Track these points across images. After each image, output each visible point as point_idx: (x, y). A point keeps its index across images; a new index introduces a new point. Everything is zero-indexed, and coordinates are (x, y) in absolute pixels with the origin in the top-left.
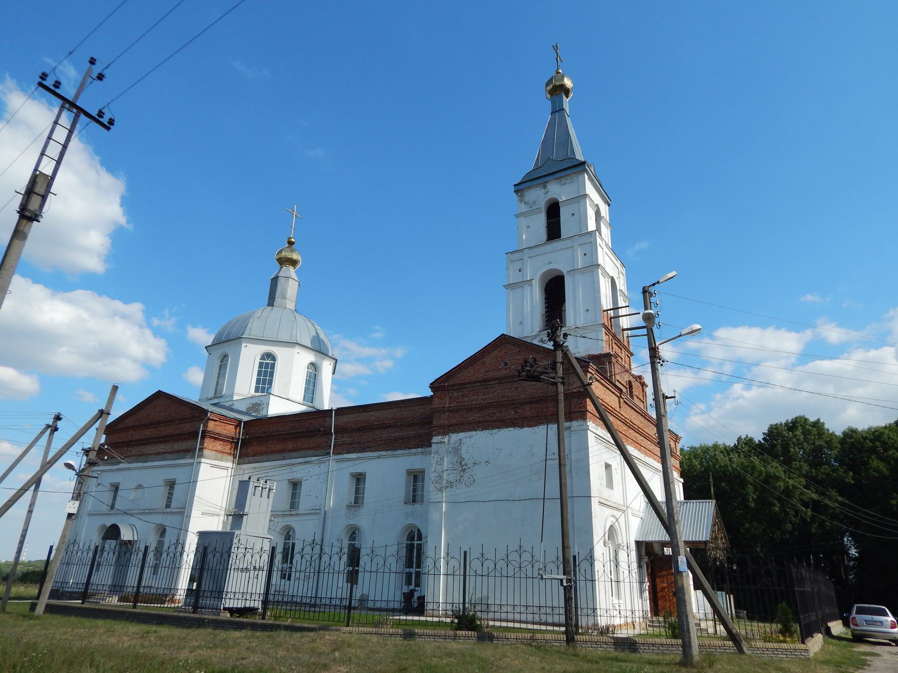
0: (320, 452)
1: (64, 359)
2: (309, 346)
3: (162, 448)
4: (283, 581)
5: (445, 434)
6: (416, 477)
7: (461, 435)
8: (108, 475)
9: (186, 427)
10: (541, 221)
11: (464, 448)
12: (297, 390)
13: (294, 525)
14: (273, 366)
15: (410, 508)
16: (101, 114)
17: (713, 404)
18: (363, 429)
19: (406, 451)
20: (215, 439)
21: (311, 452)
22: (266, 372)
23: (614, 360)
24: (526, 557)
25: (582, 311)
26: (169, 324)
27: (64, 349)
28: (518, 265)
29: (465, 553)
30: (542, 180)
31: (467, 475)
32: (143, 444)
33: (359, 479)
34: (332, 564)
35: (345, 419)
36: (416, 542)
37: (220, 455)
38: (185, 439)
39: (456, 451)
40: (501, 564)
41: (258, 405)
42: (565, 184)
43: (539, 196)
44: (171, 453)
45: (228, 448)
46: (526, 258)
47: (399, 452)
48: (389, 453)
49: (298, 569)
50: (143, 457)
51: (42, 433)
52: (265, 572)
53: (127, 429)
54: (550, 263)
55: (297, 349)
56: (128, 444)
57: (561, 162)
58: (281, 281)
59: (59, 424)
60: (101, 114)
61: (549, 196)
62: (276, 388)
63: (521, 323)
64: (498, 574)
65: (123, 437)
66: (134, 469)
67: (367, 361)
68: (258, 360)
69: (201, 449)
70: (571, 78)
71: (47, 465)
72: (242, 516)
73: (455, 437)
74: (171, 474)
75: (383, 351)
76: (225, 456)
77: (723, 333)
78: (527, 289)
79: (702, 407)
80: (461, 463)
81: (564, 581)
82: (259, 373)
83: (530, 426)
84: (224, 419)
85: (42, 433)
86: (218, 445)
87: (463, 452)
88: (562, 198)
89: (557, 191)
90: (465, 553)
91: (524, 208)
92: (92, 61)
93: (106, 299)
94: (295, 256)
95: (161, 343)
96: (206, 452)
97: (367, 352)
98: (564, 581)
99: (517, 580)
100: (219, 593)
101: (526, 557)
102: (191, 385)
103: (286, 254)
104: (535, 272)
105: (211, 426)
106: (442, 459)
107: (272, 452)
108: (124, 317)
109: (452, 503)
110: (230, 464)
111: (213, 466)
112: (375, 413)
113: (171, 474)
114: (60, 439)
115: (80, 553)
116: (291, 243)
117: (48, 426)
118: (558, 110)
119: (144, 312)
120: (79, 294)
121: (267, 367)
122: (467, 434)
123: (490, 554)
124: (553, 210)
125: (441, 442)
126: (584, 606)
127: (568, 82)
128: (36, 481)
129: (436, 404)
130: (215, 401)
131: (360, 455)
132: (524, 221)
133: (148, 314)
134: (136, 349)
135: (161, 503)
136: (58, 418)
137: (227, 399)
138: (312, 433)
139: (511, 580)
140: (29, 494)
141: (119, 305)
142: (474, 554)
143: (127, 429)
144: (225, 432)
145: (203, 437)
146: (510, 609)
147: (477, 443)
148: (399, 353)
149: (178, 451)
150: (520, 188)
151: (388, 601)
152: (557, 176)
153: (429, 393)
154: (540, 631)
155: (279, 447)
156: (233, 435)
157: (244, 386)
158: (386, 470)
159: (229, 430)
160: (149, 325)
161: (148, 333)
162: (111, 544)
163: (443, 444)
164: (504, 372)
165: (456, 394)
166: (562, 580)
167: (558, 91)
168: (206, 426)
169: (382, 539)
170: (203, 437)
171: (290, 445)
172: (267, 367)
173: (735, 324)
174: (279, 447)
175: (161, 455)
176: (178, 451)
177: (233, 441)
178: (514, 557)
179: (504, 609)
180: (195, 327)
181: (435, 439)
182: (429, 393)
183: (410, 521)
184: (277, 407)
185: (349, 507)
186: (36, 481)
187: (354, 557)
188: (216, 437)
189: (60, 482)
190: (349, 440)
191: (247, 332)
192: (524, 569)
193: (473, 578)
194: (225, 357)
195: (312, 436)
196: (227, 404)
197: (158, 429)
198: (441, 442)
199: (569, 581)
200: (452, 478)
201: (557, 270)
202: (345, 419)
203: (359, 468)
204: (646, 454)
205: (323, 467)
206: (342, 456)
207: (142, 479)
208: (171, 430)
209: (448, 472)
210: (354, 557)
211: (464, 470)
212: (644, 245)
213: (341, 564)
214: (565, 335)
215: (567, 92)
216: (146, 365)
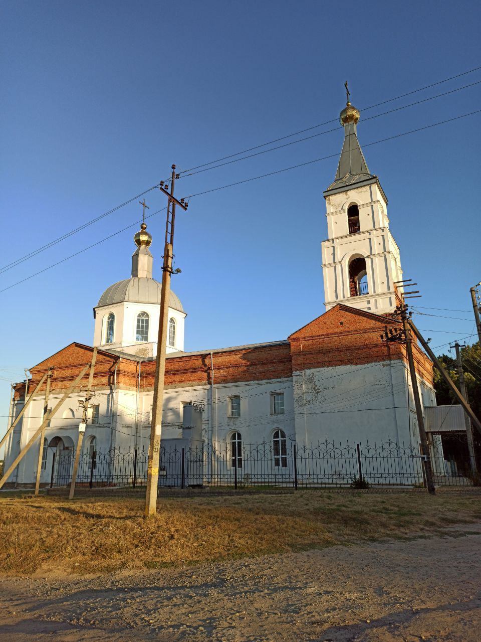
2: (182, 310)
7: (313, 370)
11: (316, 379)
14: (147, 321)
16: (182, 200)
22: (142, 326)
31: (319, 396)
34: (252, 455)
36: (237, 441)
37: (128, 387)
39: (310, 380)
40: (379, 451)
41: (145, 350)
42: (361, 192)
45: (132, 382)
54: (354, 250)
60: (182, 200)
73: (308, 372)
80: (314, 388)
81: (426, 458)
86: (126, 380)
90: (358, 445)
92: (174, 167)
96: (121, 385)
98: (426, 458)
115: (121, 456)
121: (143, 322)
122: (318, 369)
123: (372, 445)
125: (299, 375)
137: (118, 346)
139: (259, 462)
142: (187, 450)
159: (132, 368)
164: (341, 328)
166: (424, 458)
177: (136, 376)
178: (261, 447)
181: (294, 373)
183: (276, 426)
187: (94, 455)
188: (126, 374)
192: (392, 453)
193: (300, 460)
198: (299, 375)
199: (428, 458)
201: (359, 254)
209: (306, 394)
210: (94, 455)
211: (317, 393)
213: (87, 459)
214: (410, 313)
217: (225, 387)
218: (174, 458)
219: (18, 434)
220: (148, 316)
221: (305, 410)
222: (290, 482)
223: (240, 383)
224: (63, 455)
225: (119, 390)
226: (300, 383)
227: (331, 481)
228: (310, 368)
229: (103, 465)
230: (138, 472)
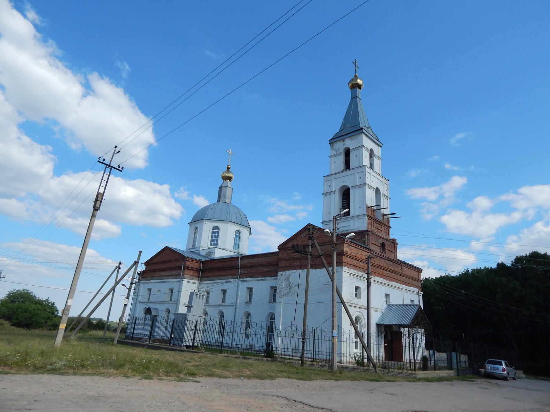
0: (234, 277)
1: (133, 216)
3: (168, 273)
4: (246, 339)
5: (283, 271)
6: (274, 290)
8: (145, 286)
9: (178, 264)
10: (341, 159)
11: (291, 278)
12: (230, 245)
13: (223, 311)
14: (218, 233)
15: (271, 305)
17: (521, 236)
18: (252, 266)
19: (270, 278)
20: (190, 270)
21: (230, 277)
22: (215, 236)
23: (369, 233)
25: (357, 207)
26: (184, 195)
27: (132, 211)
28: (329, 183)
30: (342, 138)
31: (292, 291)
32: (161, 271)
33: (251, 290)
35: (245, 261)
37: (192, 277)
38: (177, 270)
39: (288, 279)
40: (258, 330)
43: (340, 146)
44: (171, 276)
45: (196, 274)
46: (333, 179)
47: (267, 278)
48: (263, 278)
49: (320, 338)
50: (161, 277)
52: (264, 336)
53: (154, 264)
55: (230, 224)
56: (154, 271)
57: (352, 127)
58: (224, 188)
59: (121, 266)
61: (346, 146)
62: (220, 244)
63: (329, 213)
65: (152, 267)
66: (157, 282)
67: (292, 213)
68: (211, 230)
70: (361, 79)
71: (117, 283)
72: (191, 307)
73: (288, 272)
74: (171, 285)
75: (301, 207)
76: (194, 278)
77: (525, 190)
78: (332, 195)
79: (515, 238)
82: (212, 237)
83: (319, 268)
84: (193, 260)
86: (191, 273)
87: (291, 280)
88: (351, 147)
89: (350, 143)
91: (333, 153)
93: (151, 183)
94: (230, 175)
95: (179, 206)
97: (292, 208)
99: (326, 342)
100: (182, 339)
102: (180, 245)
103: (226, 174)
104: (336, 185)
105: (188, 263)
106: (282, 283)
107: (215, 276)
108: (160, 192)
109: (286, 303)
110: (197, 281)
111: (189, 282)
112: (257, 259)
113: (171, 285)
116: (228, 168)
117: (117, 267)
118: (354, 98)
119: (169, 189)
120: (138, 182)
124: (347, 153)
126: (317, 350)
127: (359, 81)
128: (113, 289)
129: (280, 256)
130: (193, 250)
131: (251, 279)
132: (333, 159)
133: (172, 191)
134: (166, 210)
135: (167, 299)
136: (120, 264)
138: (231, 268)
139: (323, 341)
140: (110, 296)
141: (157, 186)
143: (154, 264)
144: (194, 266)
146: (286, 350)
147: (296, 276)
148: (310, 208)
149: (174, 275)
150: (332, 142)
151: (242, 345)
152: (349, 135)
153: (277, 250)
154: (287, 358)
155: (217, 274)
156: (198, 268)
157: (205, 243)
158: (261, 286)
160: (173, 197)
161: (172, 201)
163: (283, 275)
165: (289, 252)
167: (355, 86)
168: (185, 263)
169: (259, 319)
170: (184, 269)
171: (222, 273)
172: (215, 233)
173: (532, 183)
174: (217, 274)
175: (167, 277)
176: (174, 275)
177: (197, 270)
179: (289, 350)
180: (198, 196)
181: (279, 273)
182: (277, 250)
184: (218, 254)
185: (246, 303)
186: (113, 289)
188: (190, 269)
189: (121, 291)
190: (246, 271)
191: (206, 216)
193: (236, 334)
194: (196, 228)
195: (231, 269)
196: (197, 252)
197: (165, 264)
200: (286, 292)
202: (245, 261)
203: (250, 285)
204: (390, 280)
205: (236, 284)
206: (243, 279)
207: (160, 286)
208: (171, 265)
211: (291, 288)
212: (461, 136)
215: (359, 86)
216: (172, 218)
217: (266, 280)
218: (320, 336)
219: (175, 305)
220: (219, 229)
221: (282, 300)
222: (309, 358)
223: (254, 279)
224: (255, 327)
225: (184, 280)
226: (128, 290)
227: (291, 354)
228: (289, 270)
229: (254, 336)
230: (308, 347)
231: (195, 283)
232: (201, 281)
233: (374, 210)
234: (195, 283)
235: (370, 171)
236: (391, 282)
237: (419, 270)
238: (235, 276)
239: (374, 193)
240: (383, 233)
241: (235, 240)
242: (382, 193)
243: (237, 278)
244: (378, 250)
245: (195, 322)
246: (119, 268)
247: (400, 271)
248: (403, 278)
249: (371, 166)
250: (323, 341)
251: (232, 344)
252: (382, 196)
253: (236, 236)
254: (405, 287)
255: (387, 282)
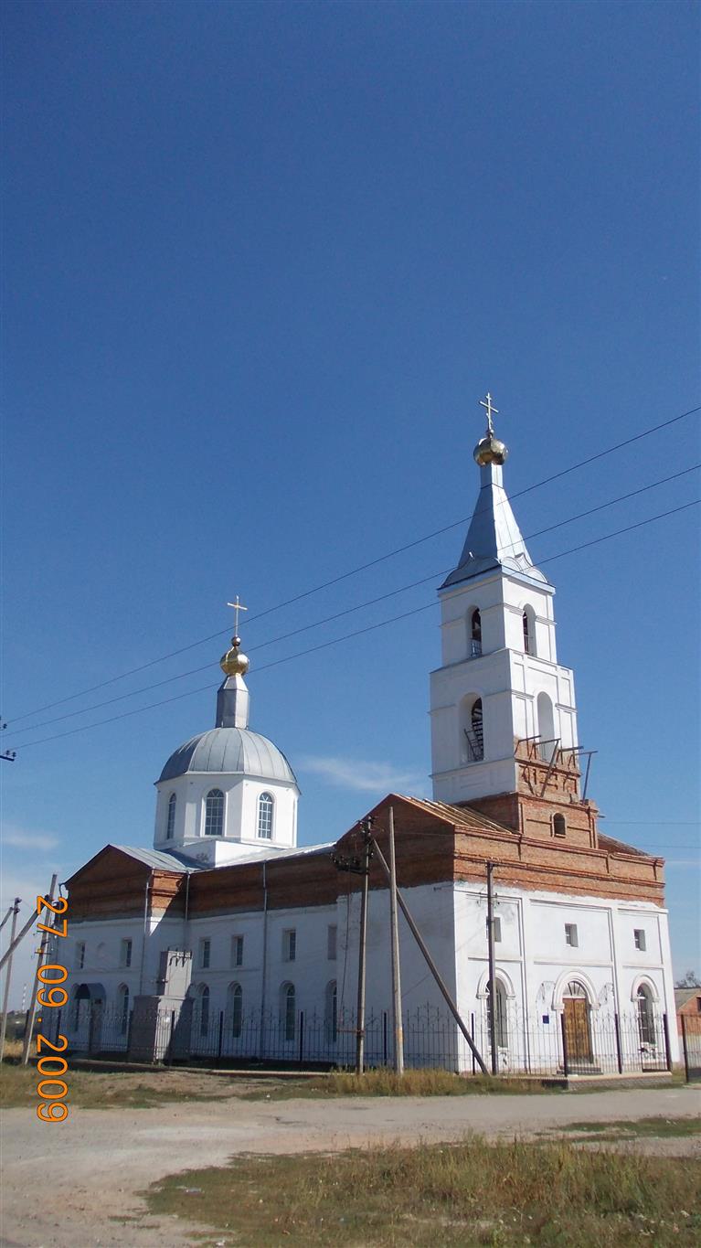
4: (235, 1038)
10: (463, 630)
22: (214, 820)
24: (433, 1012)
29: (302, 1013)
50: (102, 915)
51: (9, 914)
64: (431, 1030)
69: (150, 907)
85: (9, 914)
90: (302, 1013)
101: (433, 1012)
105: (157, 883)
114: (23, 919)
117: (11, 908)
136: (18, 901)
139: (441, 1035)
145: (150, 895)
158: (310, 923)
162: (84, 1003)
168: (151, 884)
178: (423, 1012)
184: (226, 855)
192: (431, 1025)
231: (178, 924)
232: (189, 919)
233: (534, 745)
234: (178, 924)
235: (527, 661)
236: (577, 897)
237: (163, 994)
238: (254, 905)
239: (533, 707)
240: (560, 790)
241: (262, 816)
242: (554, 701)
243: (263, 910)
244: (545, 833)
245: (170, 1014)
246: (17, 911)
247: (604, 871)
248: (614, 886)
249: (530, 648)
250: (375, 1034)
251: (301, 1058)
252: (554, 708)
253: (263, 806)
254: (614, 904)
255: (566, 898)
